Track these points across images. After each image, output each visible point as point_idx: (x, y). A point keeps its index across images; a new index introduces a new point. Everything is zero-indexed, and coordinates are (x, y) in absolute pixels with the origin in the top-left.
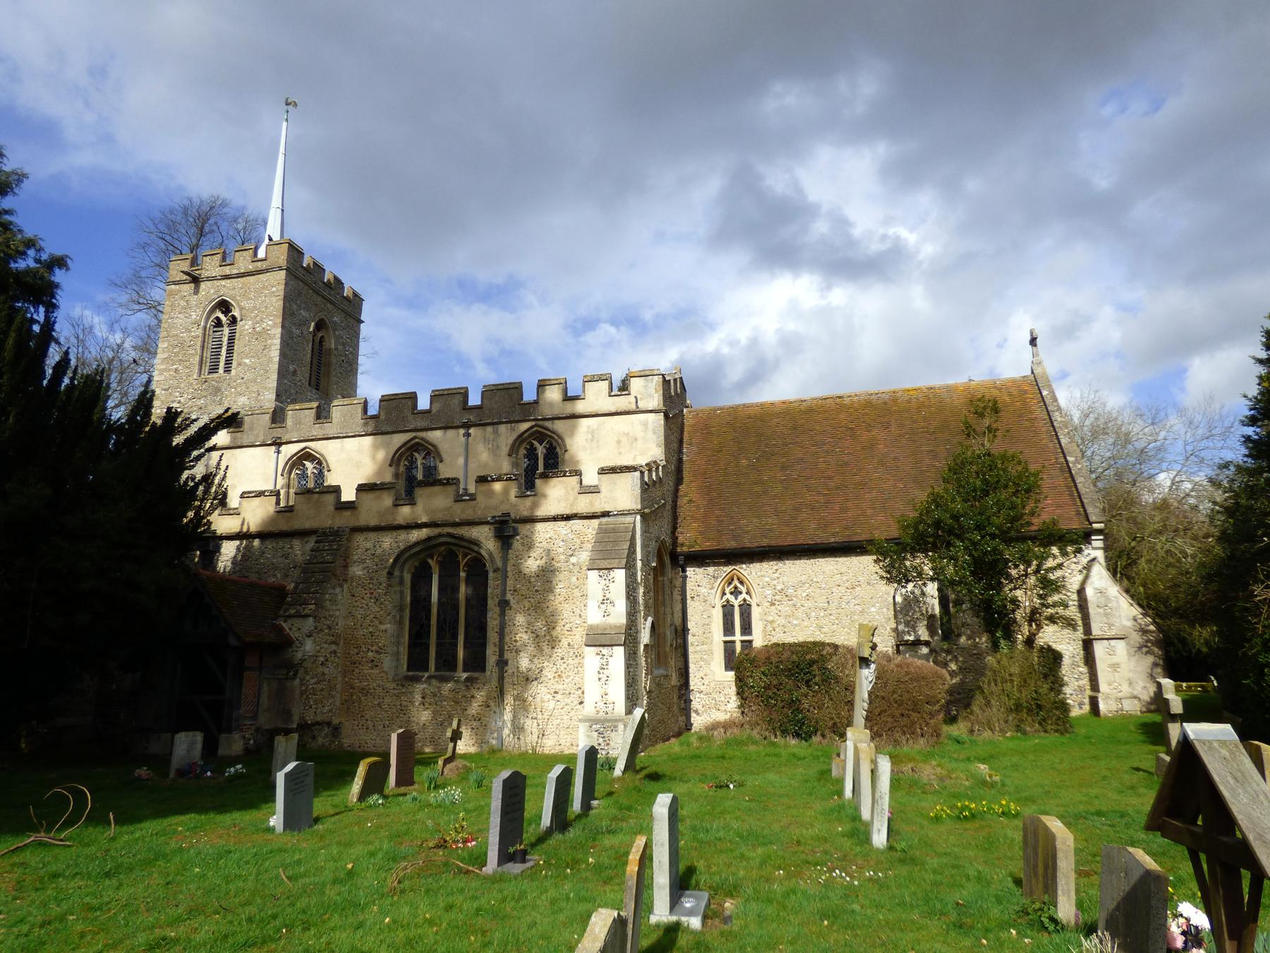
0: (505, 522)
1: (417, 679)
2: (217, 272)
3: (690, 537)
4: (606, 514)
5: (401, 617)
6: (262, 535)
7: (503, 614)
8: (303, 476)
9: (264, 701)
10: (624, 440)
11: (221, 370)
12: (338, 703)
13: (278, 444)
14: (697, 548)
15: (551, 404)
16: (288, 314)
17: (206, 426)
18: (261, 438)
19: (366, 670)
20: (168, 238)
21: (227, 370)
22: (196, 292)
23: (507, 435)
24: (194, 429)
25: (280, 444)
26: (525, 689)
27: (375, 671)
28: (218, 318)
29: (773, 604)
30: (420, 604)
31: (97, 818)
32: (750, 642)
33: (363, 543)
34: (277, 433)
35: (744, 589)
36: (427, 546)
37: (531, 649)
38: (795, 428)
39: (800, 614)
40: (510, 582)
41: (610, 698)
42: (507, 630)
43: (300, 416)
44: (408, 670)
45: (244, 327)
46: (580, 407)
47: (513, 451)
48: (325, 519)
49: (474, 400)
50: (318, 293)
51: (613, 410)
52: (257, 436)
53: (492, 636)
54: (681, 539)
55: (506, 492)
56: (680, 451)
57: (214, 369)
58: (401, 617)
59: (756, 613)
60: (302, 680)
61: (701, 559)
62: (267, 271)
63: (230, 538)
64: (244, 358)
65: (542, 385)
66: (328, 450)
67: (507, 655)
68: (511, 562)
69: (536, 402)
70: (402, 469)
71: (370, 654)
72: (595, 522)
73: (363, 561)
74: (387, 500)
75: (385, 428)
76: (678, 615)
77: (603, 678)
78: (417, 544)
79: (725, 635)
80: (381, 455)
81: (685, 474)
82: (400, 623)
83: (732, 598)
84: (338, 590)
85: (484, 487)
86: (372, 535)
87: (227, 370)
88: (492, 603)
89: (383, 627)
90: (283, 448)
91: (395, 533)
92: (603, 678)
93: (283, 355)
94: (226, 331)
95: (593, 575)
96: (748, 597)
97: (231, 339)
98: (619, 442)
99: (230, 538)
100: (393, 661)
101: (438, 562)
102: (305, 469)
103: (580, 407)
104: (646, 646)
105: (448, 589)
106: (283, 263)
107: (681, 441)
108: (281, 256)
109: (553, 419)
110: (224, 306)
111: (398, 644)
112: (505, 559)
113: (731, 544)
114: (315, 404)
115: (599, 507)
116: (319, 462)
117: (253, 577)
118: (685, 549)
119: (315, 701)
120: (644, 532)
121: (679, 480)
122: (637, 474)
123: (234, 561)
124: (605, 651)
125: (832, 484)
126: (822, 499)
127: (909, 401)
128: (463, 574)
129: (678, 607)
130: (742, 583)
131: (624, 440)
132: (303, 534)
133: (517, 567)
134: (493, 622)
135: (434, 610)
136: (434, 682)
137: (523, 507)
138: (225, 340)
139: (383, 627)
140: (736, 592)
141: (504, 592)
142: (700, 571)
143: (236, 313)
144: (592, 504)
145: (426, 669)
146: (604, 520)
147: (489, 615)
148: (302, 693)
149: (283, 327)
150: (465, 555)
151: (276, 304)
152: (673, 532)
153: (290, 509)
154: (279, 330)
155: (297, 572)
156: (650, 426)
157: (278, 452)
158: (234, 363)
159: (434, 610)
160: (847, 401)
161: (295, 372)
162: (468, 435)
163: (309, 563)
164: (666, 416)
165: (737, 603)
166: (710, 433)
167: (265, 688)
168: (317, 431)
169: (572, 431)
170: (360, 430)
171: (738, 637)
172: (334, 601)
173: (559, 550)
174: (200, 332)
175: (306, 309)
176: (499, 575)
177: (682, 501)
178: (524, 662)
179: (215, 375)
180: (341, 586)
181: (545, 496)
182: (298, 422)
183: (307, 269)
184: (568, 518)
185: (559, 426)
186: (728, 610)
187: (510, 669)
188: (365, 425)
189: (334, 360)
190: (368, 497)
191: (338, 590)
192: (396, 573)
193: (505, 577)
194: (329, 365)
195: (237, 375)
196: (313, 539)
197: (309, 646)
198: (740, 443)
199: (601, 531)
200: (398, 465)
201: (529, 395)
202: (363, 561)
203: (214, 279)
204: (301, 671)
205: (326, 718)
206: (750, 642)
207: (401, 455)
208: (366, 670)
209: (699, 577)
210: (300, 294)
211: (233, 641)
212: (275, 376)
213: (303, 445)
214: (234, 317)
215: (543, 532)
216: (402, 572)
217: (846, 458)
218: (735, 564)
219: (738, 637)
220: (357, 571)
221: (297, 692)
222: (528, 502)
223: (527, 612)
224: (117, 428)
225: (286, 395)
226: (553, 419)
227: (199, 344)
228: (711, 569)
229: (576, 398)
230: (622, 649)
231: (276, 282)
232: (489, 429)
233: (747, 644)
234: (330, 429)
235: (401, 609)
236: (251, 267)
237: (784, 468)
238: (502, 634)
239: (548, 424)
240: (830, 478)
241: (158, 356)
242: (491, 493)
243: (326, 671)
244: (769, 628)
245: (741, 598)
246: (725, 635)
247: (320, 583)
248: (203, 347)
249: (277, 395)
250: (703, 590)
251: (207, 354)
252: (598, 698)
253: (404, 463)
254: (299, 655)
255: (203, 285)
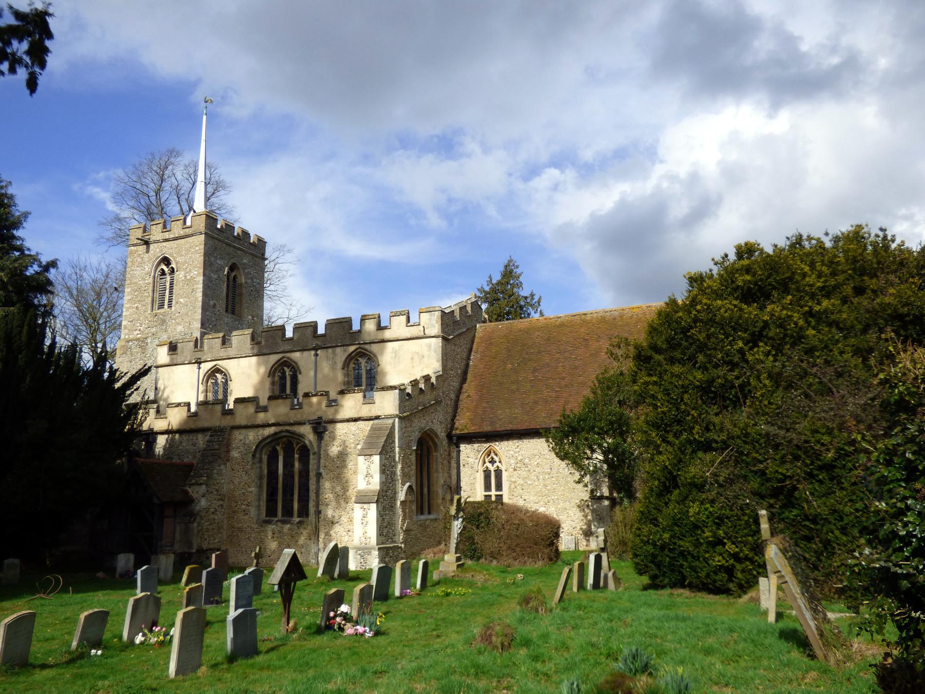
0: (319, 423)
1: (269, 522)
2: (160, 236)
3: (463, 423)
4: (377, 418)
5: (261, 483)
6: (180, 431)
7: (318, 481)
8: (216, 384)
9: (178, 536)
10: (416, 357)
11: (166, 307)
12: (225, 537)
13: (199, 362)
14: (466, 431)
15: (369, 333)
16: (208, 265)
17: (133, 376)
18: (189, 358)
19: (241, 516)
20: (139, 186)
21: (170, 306)
22: (148, 251)
23: (341, 354)
24: (125, 379)
25: (200, 363)
26: (331, 528)
27: (246, 517)
28: (162, 270)
29: (515, 470)
30: (272, 474)
31: (65, 590)
32: (501, 496)
33: (238, 436)
34: (199, 355)
35: (496, 459)
36: (275, 438)
37: (333, 504)
38: (548, 339)
39: (533, 477)
40: (322, 461)
41: (368, 535)
42: (321, 492)
43: (213, 342)
44: (267, 516)
45: (179, 275)
46: (387, 334)
47: (346, 365)
48: (215, 420)
49: (321, 330)
50: (230, 245)
51: (409, 336)
52: (186, 357)
53: (312, 495)
54: (457, 424)
55: (319, 403)
56: (468, 358)
57: (161, 306)
58: (261, 483)
59: (505, 476)
60: (199, 523)
61: (470, 438)
62: (192, 235)
63: (162, 433)
64: (180, 299)
65: (363, 319)
66: (231, 366)
67: (321, 507)
68: (323, 448)
69: (360, 331)
70: (277, 378)
71: (243, 507)
72: (371, 422)
73: (238, 448)
74: (251, 409)
75: (265, 351)
76: (454, 477)
77: (364, 524)
78: (269, 437)
79: (486, 491)
80: (262, 370)
81: (469, 376)
82: (260, 487)
83: (489, 465)
84: (223, 467)
85: (306, 401)
86: (243, 431)
87: (170, 306)
88: (312, 474)
89: (250, 490)
90: (202, 365)
91: (256, 430)
92: (364, 524)
93: (205, 294)
94: (168, 278)
95: (361, 459)
96: (500, 465)
97: (172, 284)
98: (412, 359)
99: (162, 433)
100: (254, 511)
101: (282, 448)
102: (216, 380)
103: (387, 334)
104: (402, 502)
105: (288, 465)
106: (203, 229)
107: (471, 350)
108: (201, 224)
109: (370, 343)
110: (166, 261)
111: (259, 500)
112: (319, 446)
113: (487, 428)
114: (221, 335)
115: (374, 413)
116: (226, 375)
117: (176, 460)
118: (458, 432)
119: (209, 536)
120: (401, 429)
121: (464, 380)
122: (397, 391)
123: (165, 448)
124: (365, 506)
125: (563, 383)
126: (554, 394)
127: (631, 318)
128: (296, 456)
129: (454, 472)
130: (496, 455)
131: (416, 357)
132: (203, 430)
133: (326, 451)
134: (312, 487)
135: (281, 479)
136: (279, 524)
137: (329, 414)
138: (168, 285)
139: (250, 490)
140: (492, 462)
141: (319, 467)
142: (469, 446)
143: (173, 265)
144: (370, 410)
145: (276, 516)
146: (376, 421)
147: (311, 482)
148: (199, 532)
149: (204, 275)
150: (298, 444)
151: (199, 259)
152: (453, 420)
153: (195, 414)
154: (202, 278)
155: (198, 455)
156: (433, 347)
157: (199, 368)
158: (174, 303)
159: (281, 479)
160: (588, 317)
161: (214, 306)
162: (316, 355)
163: (205, 450)
164: (445, 339)
165: (492, 468)
166: (491, 344)
167: (178, 528)
168: (223, 353)
169: (382, 351)
170: (249, 352)
171: (493, 493)
172: (220, 474)
173: (351, 441)
174: (151, 280)
175: (222, 259)
176: (316, 457)
177: (462, 397)
178: (330, 512)
179: (162, 311)
180: (225, 464)
181: (342, 406)
182: (211, 348)
183: (221, 230)
184: (356, 420)
185: (374, 348)
186: (487, 474)
187: (322, 516)
188: (252, 349)
189: (244, 291)
190: (241, 407)
191: (223, 467)
192: (257, 456)
193: (319, 458)
194: (241, 295)
195: (176, 310)
196: (209, 433)
197: (203, 503)
198: (509, 351)
199: (373, 429)
200: (274, 376)
201: (356, 327)
202: (238, 448)
203: (158, 241)
204: (198, 519)
205: (216, 546)
206: (501, 496)
207: (275, 370)
208: (241, 516)
209: (469, 451)
210: (216, 249)
211: (156, 501)
212: (200, 311)
213: (214, 363)
214: (173, 268)
215: (341, 429)
216: (261, 455)
217: (577, 363)
218: (491, 442)
219: (493, 493)
220: (235, 454)
221: (196, 530)
222: (332, 410)
223: (331, 480)
224: (87, 373)
225: (208, 324)
226: (370, 343)
227: (151, 289)
228: (476, 446)
229: (385, 328)
230: (375, 505)
231: (199, 242)
232: (330, 350)
233: (499, 497)
234: (231, 352)
235: (261, 478)
236: (182, 233)
237: (535, 370)
238: (318, 494)
239: (367, 347)
240: (563, 378)
241: (125, 298)
242: (311, 404)
243: (216, 517)
244: (513, 486)
245: (495, 465)
246: (486, 491)
247: (210, 463)
248: (153, 291)
249: (202, 324)
250: (471, 460)
251: (157, 295)
252: (361, 535)
253: (278, 374)
254: (198, 508)
255: (152, 246)
